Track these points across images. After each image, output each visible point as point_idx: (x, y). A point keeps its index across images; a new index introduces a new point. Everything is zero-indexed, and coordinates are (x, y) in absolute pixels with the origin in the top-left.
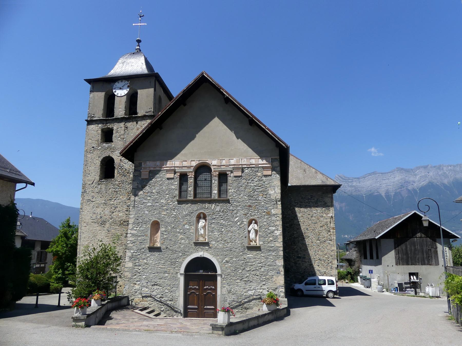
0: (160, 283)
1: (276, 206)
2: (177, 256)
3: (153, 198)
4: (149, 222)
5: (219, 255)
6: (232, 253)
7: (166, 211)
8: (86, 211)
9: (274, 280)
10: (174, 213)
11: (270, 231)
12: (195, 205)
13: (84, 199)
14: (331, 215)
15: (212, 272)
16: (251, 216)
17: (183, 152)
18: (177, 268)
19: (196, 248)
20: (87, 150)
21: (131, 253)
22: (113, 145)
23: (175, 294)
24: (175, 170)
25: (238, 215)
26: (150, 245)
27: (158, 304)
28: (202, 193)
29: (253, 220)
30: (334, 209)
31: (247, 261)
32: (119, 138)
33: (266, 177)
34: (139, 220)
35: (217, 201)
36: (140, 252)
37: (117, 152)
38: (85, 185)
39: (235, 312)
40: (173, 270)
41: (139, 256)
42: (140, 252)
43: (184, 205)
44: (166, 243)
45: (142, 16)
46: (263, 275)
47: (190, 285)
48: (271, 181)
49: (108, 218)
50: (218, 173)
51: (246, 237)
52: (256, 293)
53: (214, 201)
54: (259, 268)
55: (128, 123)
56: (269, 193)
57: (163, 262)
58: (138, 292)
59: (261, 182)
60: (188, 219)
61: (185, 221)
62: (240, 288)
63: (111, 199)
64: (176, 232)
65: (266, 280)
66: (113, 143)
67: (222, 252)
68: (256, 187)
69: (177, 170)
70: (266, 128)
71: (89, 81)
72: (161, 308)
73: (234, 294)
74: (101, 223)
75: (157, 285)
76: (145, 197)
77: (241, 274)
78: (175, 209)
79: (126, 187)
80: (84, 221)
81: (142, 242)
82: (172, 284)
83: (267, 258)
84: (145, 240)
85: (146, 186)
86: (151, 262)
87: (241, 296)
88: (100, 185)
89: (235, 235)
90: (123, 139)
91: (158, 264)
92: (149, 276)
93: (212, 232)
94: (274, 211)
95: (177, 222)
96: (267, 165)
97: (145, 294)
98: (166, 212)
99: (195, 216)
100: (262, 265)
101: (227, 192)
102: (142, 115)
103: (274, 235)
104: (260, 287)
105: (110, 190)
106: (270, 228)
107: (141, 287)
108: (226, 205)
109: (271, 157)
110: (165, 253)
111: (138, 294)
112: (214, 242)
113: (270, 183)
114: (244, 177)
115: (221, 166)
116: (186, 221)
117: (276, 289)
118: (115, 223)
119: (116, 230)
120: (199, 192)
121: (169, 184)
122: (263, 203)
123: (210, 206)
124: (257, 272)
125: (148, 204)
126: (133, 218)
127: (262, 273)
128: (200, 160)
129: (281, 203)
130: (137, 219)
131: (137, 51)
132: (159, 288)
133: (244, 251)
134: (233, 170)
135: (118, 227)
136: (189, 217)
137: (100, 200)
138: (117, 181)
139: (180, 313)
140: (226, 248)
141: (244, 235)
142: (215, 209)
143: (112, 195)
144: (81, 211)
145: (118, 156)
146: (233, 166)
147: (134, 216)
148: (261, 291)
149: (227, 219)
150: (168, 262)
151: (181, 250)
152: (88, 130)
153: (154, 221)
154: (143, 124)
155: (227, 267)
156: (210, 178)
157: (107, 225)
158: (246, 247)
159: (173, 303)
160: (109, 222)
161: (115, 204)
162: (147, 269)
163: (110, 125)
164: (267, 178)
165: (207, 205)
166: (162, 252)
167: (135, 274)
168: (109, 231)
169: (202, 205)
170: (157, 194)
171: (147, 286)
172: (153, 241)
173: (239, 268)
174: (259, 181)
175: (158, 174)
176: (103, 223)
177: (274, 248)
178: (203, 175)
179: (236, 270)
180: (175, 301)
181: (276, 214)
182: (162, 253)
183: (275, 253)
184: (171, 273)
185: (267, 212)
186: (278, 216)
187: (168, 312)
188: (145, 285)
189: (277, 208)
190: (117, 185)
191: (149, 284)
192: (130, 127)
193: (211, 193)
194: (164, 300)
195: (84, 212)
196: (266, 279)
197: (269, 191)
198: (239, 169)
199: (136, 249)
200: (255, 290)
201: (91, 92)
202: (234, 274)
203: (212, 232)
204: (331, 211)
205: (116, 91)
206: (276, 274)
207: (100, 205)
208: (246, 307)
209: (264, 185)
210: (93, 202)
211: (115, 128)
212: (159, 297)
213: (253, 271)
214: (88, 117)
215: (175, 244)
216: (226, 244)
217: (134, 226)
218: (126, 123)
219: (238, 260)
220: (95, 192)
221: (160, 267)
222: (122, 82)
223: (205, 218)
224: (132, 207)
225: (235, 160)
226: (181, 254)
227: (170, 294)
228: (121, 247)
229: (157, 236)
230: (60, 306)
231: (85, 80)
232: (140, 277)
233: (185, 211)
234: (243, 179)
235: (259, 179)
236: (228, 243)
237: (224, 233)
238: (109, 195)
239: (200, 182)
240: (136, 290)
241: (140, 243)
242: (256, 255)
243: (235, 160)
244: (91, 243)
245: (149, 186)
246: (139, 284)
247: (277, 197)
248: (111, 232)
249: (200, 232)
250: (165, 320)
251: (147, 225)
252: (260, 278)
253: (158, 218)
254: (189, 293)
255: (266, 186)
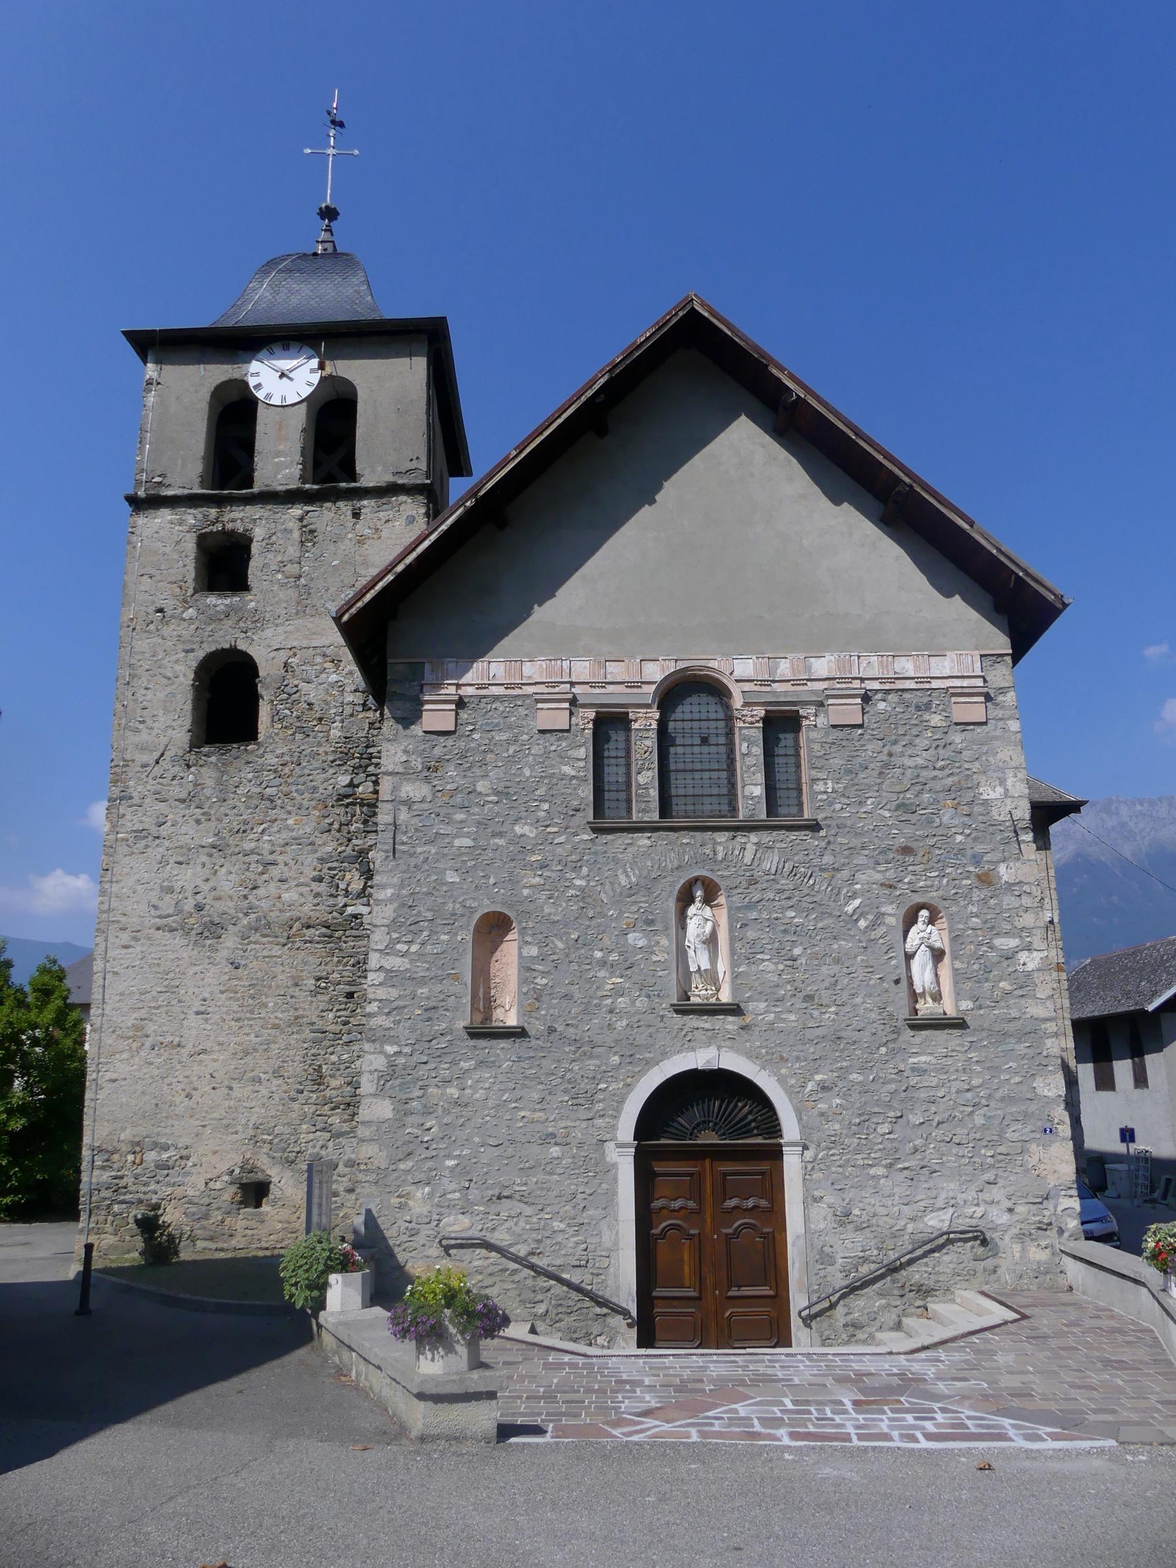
0: (524, 1188)
4: (465, 918)
6: (843, 1050)
10: (578, 882)
20: (132, 619)
21: (387, 1056)
22: (251, 601)
25: (858, 886)
26: (472, 1023)
29: (923, 906)
31: (912, 1083)
32: (280, 576)
34: (417, 909)
36: (427, 1052)
37: (267, 631)
42: (427, 1052)
44: (548, 1009)
46: (985, 1144)
48: (985, 748)
51: (897, 982)
52: (960, 1221)
56: (982, 797)
60: (641, 905)
68: (924, 773)
76: (443, 811)
79: (311, 777)
80: (118, 922)
88: (193, 769)
91: (514, 1105)
93: (750, 959)
94: (1009, 871)
106: (998, 942)
110: (542, 1055)
112: (762, 1005)
115: (774, 681)
116: (631, 916)
118: (265, 932)
120: (679, 794)
121: (547, 754)
122: (959, 838)
124: (958, 1131)
125: (457, 843)
126: (390, 900)
127: (978, 1136)
136: (644, 899)
142: (756, 863)
149: (813, 905)
157: (230, 941)
161: (266, 853)
168: (236, 968)
170: (495, 798)
184: (574, 1143)
191: (474, 1194)
192: (329, 529)
195: (120, 885)
203: (750, 959)
208: (922, 1285)
211: (258, 533)
214: (139, 483)
216: (816, 1013)
217: (395, 935)
227: (575, 1239)
228: (295, 1036)
232: (430, 1164)
240: (413, 1225)
241: (426, 1010)
244: (155, 1018)
251: (456, 934)
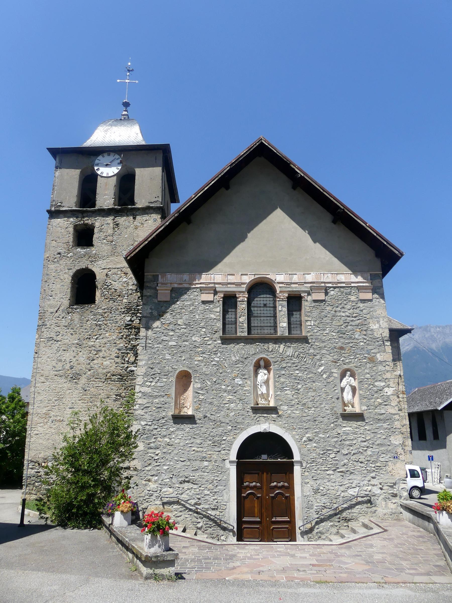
0: (193, 478)
1: (384, 349)
2: (223, 430)
3: (178, 333)
4: (172, 373)
5: (295, 429)
6: (317, 425)
7: (201, 355)
8: (45, 357)
9: (390, 469)
11: (378, 388)
12: (251, 346)
13: (41, 337)
14: (400, 372)
15: (282, 457)
16: (344, 364)
17: (227, 260)
18: (224, 451)
19: (255, 417)
21: (142, 426)
22: (93, 250)
23: (222, 498)
24: (216, 289)
27: (192, 516)
28: (261, 326)
30: (403, 364)
32: (105, 241)
33: (363, 303)
34: (154, 369)
35: (287, 339)
37: (100, 262)
38: (44, 313)
39: (329, 527)
40: (218, 456)
41: (155, 432)
43: (232, 345)
44: (204, 408)
45: (132, 71)
46: (371, 462)
47: (245, 481)
48: (372, 309)
49: (84, 369)
50: (287, 295)
52: (361, 492)
53: (283, 339)
54: (363, 450)
55: (119, 217)
56: (370, 328)
57: (198, 441)
58: (155, 494)
59: (357, 311)
61: (235, 372)
62: (335, 485)
63: (89, 337)
64: (220, 390)
65: (376, 469)
66: (94, 247)
67: (300, 424)
68: (348, 318)
69: (219, 288)
70: (367, 225)
71: (54, 152)
72: (198, 523)
73: (324, 495)
74: (72, 377)
75: (188, 482)
76: (165, 331)
77: (334, 460)
78: (217, 352)
79: (115, 318)
80: (40, 373)
81: (160, 407)
82: (217, 480)
83: (376, 432)
84: (166, 403)
85: (165, 312)
86: (177, 441)
87: (336, 498)
88: (70, 314)
89: (319, 396)
90: (112, 242)
91: (190, 445)
92: (175, 467)
95: (221, 373)
96: (364, 285)
97: (167, 498)
98: (202, 357)
99: (252, 363)
100: (368, 445)
101: (301, 325)
102: (144, 206)
103: (383, 395)
104: (368, 482)
105: (87, 323)
106: (376, 384)
107: (161, 486)
108: (303, 345)
109: (369, 272)
110: (202, 426)
111: (155, 498)
112: (286, 407)
113: (370, 312)
114: (329, 302)
115: (292, 283)
116: (236, 372)
117: (395, 484)
118: (96, 377)
119: (97, 389)
121: (205, 310)
122: (362, 344)
123: (277, 348)
124: (361, 457)
125: (170, 343)
127: (369, 459)
128: (257, 273)
129: (391, 344)
130: (152, 368)
131: (125, 118)
132: (192, 488)
133: (337, 421)
134: (311, 291)
135: (102, 383)
137: (71, 338)
138: (101, 308)
139: (232, 531)
140: (307, 416)
141: (335, 394)
142: (284, 352)
143: (92, 330)
144: (36, 356)
145: (103, 269)
146: (311, 285)
147: (145, 363)
148: (369, 488)
149: (306, 369)
150: (208, 441)
151: (230, 421)
152: (50, 226)
153: (182, 371)
154: (145, 220)
155: (309, 449)
156: (272, 302)
157: (83, 380)
158: (339, 415)
159: (218, 513)
160: (85, 376)
161: (97, 346)
162: (170, 453)
163: (88, 220)
164: (365, 304)
165: (271, 346)
166: (196, 424)
167: (149, 462)
168: (85, 391)
169: (263, 346)
170: (185, 327)
171: (171, 484)
172: (178, 406)
173: (331, 450)
174: (354, 308)
175: (186, 293)
176: (76, 377)
177: (385, 415)
178: (260, 298)
179: (325, 453)
180: (223, 511)
181: (384, 362)
182: (197, 425)
183: (388, 425)
184: (213, 460)
185: (369, 358)
186: (387, 365)
187: (210, 530)
188: (168, 483)
189: (385, 351)
190: (100, 315)
191: (174, 480)
193: (275, 327)
194: (203, 508)
196: (377, 468)
197: (370, 325)
198: (321, 289)
199: (149, 418)
200: (359, 487)
201: (58, 169)
202: (323, 460)
203: (282, 389)
204: (399, 367)
205: (99, 169)
206: (392, 459)
207: (70, 346)
208: (347, 517)
209: (361, 315)
210: (57, 341)
211: (97, 224)
212: (192, 504)
213: (354, 454)
214: (52, 206)
215: (219, 410)
216: (306, 411)
217: (146, 379)
218: (116, 217)
219: (328, 437)
220: (62, 326)
221: (194, 450)
222: (109, 155)
223: (267, 366)
224: (141, 348)
225: (313, 275)
226: (230, 427)
227: (213, 498)
229: (185, 397)
230: (24, 525)
231: (47, 149)
232: (158, 468)
233: (234, 355)
234: (327, 306)
235: (353, 306)
236: (309, 408)
237: (301, 392)
238: (86, 331)
239: (256, 309)
240: (151, 492)
241: (157, 408)
242: (356, 428)
243: (313, 275)
245: (171, 313)
246: (155, 481)
247: (384, 335)
248: (89, 393)
249: (260, 390)
250: (246, 548)
251: (169, 379)
252: (366, 466)
253: (188, 367)
254: (245, 495)
255: (365, 317)
